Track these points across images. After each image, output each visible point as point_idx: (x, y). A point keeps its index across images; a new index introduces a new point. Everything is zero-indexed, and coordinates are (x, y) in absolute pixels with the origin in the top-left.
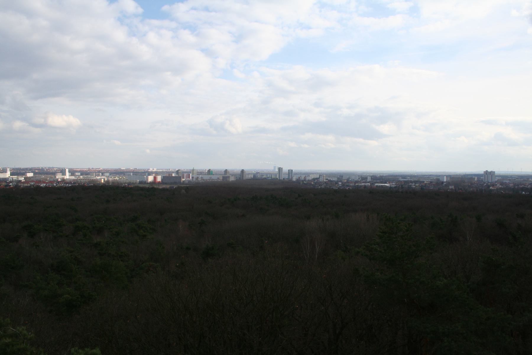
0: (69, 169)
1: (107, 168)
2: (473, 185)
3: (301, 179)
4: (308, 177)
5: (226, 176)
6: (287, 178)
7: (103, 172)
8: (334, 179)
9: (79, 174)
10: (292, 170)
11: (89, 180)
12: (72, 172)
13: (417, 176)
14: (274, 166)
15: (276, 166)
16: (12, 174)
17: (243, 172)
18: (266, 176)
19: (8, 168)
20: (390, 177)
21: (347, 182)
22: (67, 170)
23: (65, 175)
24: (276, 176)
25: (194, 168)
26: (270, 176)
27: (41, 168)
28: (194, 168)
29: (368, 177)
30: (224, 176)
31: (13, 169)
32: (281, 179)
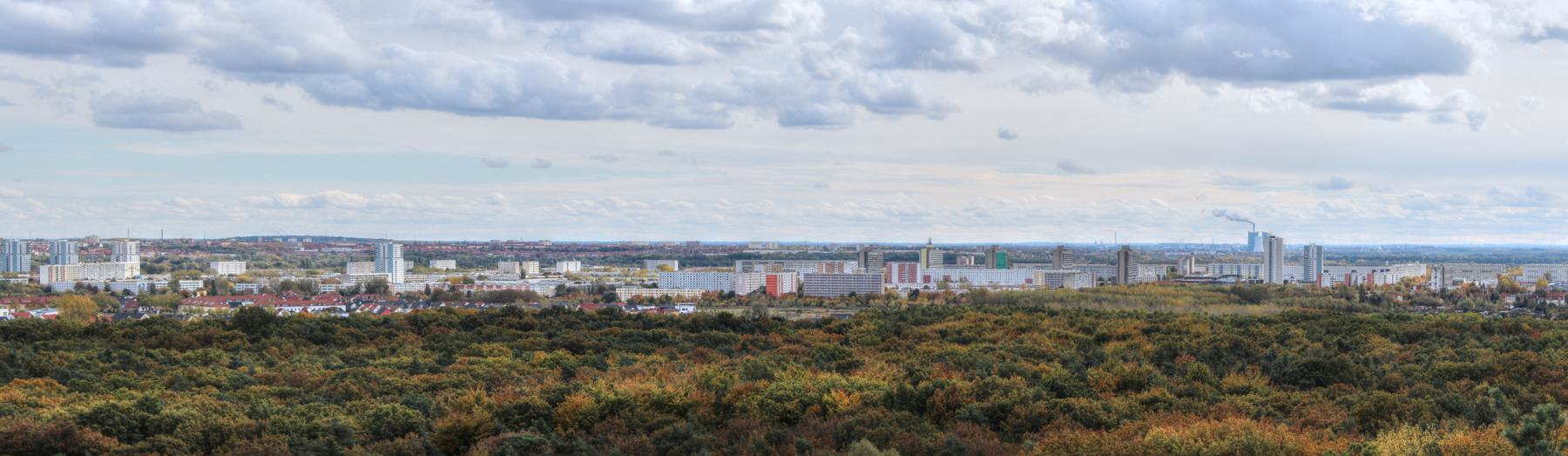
0: (405, 245)
1: (628, 240)
2: (724, 362)
3: (1356, 282)
4: (1385, 273)
5: (1061, 271)
6: (1302, 278)
7: (548, 255)
8: (1486, 283)
9: (452, 264)
10: (1319, 248)
11: (495, 288)
12: (420, 255)
13: (1542, 250)
14: (1252, 231)
15: (1257, 234)
16: (147, 268)
17: (1126, 254)
18: (1217, 271)
19: (132, 240)
20: (899, 251)
21: (1537, 292)
22: (398, 251)
23: (390, 270)
24: (1257, 273)
25: (930, 240)
26: (1235, 273)
27: (209, 243)
28: (930, 240)
29: (973, 263)
30: (1052, 272)
31: (158, 245)
32: (1275, 280)
